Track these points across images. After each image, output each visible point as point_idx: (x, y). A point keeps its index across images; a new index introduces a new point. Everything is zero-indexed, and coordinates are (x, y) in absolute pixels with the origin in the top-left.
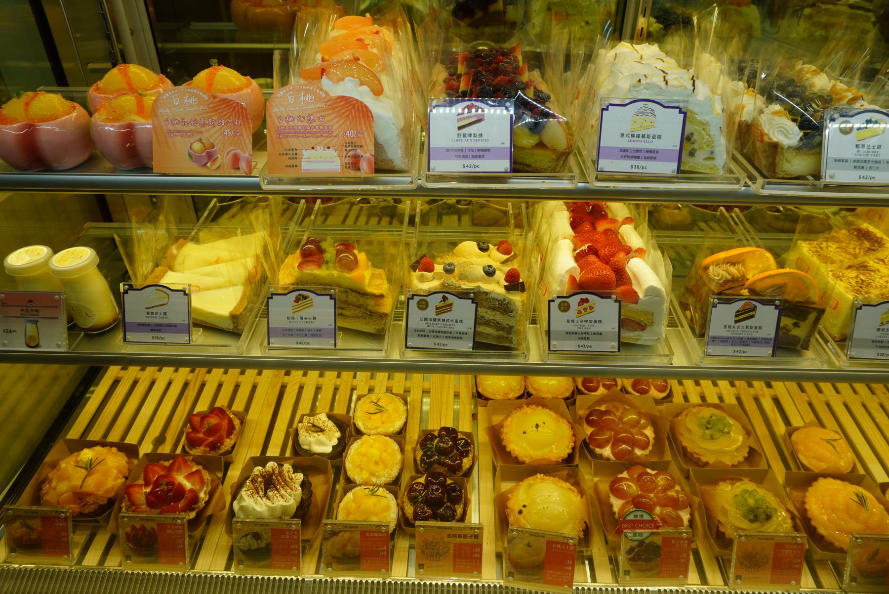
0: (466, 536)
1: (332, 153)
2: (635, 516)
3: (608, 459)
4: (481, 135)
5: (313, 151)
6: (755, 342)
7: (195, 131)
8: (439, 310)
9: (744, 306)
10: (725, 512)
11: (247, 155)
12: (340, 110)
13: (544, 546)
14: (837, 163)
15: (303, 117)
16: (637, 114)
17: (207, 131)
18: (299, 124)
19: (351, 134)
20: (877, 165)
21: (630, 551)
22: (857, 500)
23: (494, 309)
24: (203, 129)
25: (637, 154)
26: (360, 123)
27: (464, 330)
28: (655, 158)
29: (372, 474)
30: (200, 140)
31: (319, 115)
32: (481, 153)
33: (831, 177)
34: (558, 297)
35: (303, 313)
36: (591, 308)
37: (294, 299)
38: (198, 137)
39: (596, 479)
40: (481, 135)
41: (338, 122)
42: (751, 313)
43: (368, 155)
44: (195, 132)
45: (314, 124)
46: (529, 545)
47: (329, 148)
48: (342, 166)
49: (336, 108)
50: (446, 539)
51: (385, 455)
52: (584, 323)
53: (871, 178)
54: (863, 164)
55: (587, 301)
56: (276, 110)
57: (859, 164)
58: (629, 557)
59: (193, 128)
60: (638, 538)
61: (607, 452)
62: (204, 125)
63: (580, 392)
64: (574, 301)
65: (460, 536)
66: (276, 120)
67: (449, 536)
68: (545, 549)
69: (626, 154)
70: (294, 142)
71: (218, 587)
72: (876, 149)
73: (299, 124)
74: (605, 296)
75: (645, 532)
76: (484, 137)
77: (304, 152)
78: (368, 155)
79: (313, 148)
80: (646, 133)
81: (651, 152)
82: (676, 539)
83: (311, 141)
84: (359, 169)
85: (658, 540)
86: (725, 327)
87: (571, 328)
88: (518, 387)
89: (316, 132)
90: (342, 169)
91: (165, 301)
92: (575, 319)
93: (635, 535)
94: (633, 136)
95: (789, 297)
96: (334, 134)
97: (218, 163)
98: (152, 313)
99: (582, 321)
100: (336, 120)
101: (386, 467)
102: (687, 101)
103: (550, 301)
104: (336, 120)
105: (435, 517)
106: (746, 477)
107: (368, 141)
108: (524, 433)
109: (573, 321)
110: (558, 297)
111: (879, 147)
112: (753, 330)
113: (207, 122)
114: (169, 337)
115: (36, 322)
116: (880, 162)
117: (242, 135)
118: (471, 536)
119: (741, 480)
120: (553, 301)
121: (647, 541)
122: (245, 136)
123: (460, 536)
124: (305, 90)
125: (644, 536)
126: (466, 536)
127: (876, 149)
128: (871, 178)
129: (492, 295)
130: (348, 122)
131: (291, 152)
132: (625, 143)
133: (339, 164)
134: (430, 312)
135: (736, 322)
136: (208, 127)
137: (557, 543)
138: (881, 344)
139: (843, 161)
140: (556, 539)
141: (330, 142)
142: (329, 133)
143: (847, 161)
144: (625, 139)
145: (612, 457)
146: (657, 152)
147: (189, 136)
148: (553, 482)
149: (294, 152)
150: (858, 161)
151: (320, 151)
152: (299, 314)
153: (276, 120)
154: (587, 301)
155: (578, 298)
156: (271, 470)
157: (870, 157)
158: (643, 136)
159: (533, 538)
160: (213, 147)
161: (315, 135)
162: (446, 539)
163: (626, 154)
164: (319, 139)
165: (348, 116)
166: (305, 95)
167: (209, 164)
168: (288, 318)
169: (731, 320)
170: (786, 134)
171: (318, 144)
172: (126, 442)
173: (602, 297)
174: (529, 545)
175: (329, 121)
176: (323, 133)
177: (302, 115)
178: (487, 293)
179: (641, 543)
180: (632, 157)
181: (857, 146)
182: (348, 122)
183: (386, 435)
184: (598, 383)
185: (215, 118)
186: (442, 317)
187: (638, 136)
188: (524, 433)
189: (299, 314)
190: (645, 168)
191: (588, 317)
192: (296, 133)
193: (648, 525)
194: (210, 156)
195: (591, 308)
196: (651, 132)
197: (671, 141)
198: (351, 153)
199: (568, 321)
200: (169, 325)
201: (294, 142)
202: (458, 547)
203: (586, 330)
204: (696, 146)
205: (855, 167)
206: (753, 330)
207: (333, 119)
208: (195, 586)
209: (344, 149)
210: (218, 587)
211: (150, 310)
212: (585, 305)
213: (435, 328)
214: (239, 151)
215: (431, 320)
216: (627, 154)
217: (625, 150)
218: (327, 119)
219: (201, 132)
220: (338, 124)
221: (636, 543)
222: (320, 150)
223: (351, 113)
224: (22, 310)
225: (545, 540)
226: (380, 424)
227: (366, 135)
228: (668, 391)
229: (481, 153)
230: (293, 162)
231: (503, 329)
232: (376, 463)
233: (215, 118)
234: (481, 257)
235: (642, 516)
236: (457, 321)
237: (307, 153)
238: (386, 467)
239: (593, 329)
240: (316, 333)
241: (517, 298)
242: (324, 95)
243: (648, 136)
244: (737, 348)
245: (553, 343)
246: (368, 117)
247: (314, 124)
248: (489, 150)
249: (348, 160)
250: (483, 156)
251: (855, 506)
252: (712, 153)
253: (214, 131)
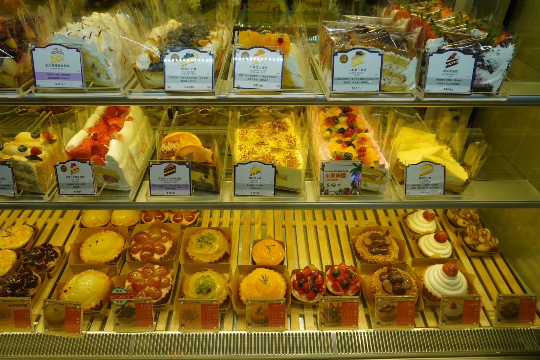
0: (19, 305)
2: (117, 291)
3: (138, 260)
6: (179, 187)
9: (168, 165)
10: (188, 288)
13: (64, 310)
14: (172, 79)
20: (195, 79)
21: (117, 312)
22: (262, 279)
23: (23, 171)
27: (7, 183)
28: (459, 84)
33: (169, 87)
34: (60, 163)
42: (174, 170)
46: (55, 310)
50: (9, 308)
53: (451, 90)
54: (186, 79)
57: (184, 79)
58: (117, 315)
60: (120, 304)
61: (137, 256)
63: (142, 222)
65: (16, 306)
67: (10, 305)
68: (64, 311)
71: (120, 347)
72: (193, 70)
74: (84, 162)
75: (124, 301)
80: (60, 63)
81: (65, 75)
82: (143, 304)
85: (133, 305)
86: (159, 178)
87: (69, 181)
88: (104, 220)
93: (118, 302)
94: (53, 65)
95: (195, 160)
102: (81, 45)
105: (12, 295)
106: (210, 268)
108: (90, 246)
110: (60, 163)
111: (195, 69)
112: (176, 180)
116: (196, 78)
118: (23, 305)
119: (207, 270)
120: (58, 166)
121: (126, 305)
123: (16, 306)
125: (124, 302)
126: (19, 305)
127: (193, 70)
128: (451, 90)
129: (19, 163)
132: (49, 70)
135: (165, 175)
137: (71, 308)
138: (252, 187)
139: (274, 77)
140: (70, 306)
143: (177, 77)
144: (48, 68)
145: (140, 259)
146: (69, 75)
148: (95, 274)
150: (183, 78)
157: (190, 75)
159: (57, 306)
162: (9, 308)
163: (251, 78)
169: (162, 174)
173: (82, 163)
174: (55, 310)
179: (123, 307)
180: (55, 78)
181: (182, 69)
183: (11, 249)
184: (152, 217)
187: (56, 66)
188: (90, 246)
190: (64, 84)
193: (125, 296)
195: (78, 169)
196: (63, 63)
197: (76, 68)
202: (16, 312)
203: (76, 182)
204: (98, 71)
205: (182, 81)
206: (176, 180)
208: (106, 347)
210: (120, 347)
212: (74, 167)
217: (50, 74)
221: (120, 307)
225: (64, 306)
226: (9, 243)
228: (193, 221)
231: (31, 183)
234: (33, 141)
235: (121, 291)
239: (80, 182)
241: (33, 165)
243: (62, 66)
244: (169, 191)
251: (260, 283)
252: (107, 75)
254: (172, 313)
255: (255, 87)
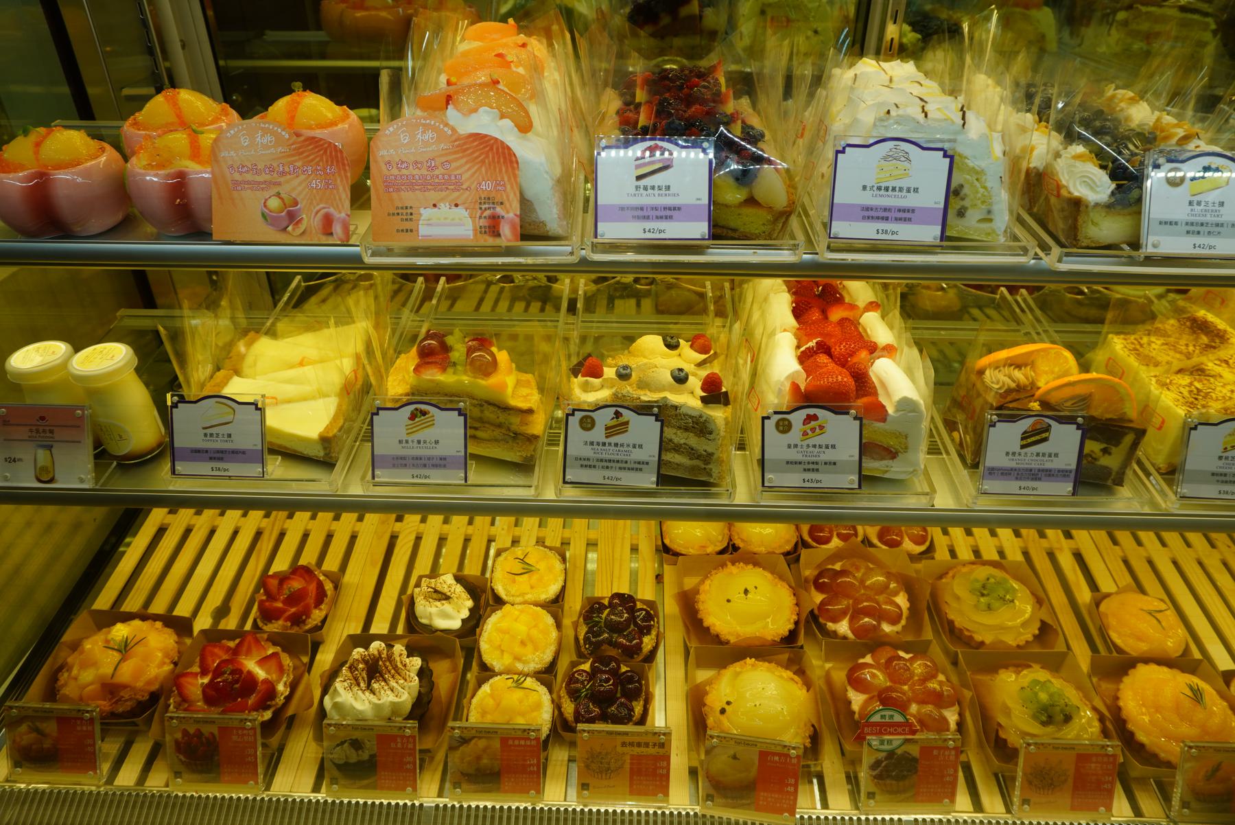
0: (647, 745)
1: (461, 212)
2: (882, 717)
3: (845, 638)
4: (668, 188)
5: (436, 210)
6: (1049, 474)
7: (270, 182)
8: (610, 431)
9: (1034, 424)
10: (1007, 712)
11: (343, 215)
12: (473, 153)
13: (756, 758)
14: (1163, 226)
15: (421, 163)
16: (885, 159)
17: (287, 182)
18: (415, 172)
19: (487, 186)
20: (1219, 229)
21: (876, 765)
22: (1190, 694)
23: (686, 429)
24: (282, 180)
25: (885, 214)
26: (501, 171)
27: (644, 458)
28: (910, 220)
29: (517, 658)
30: (278, 195)
31: (444, 159)
32: (668, 213)
33: (1155, 246)
34: (776, 413)
35: (420, 435)
36: (821, 427)
37: (409, 415)
38: (275, 190)
39: (828, 665)
40: (668, 188)
41: (469, 169)
42: (1044, 435)
43: (511, 215)
44: (270, 184)
45: (437, 172)
46: (735, 757)
47: (456, 205)
48: (475, 230)
49: (467, 149)
50: (620, 749)
51: (534, 632)
52: (811, 449)
53: (1210, 247)
54: (1199, 228)
55: (815, 417)
56: (383, 152)
57: (1194, 228)
58: (874, 773)
59: (268, 177)
60: (886, 747)
61: (843, 627)
62: (283, 173)
63: (806, 545)
64: (797, 418)
65: (639, 745)
66: (384, 167)
67: (624, 744)
68: (757, 762)
69: (869, 213)
70: (408, 198)
72: (1217, 208)
73: (415, 172)
74: (840, 411)
75: (897, 739)
76: (672, 190)
77: (422, 211)
78: (511, 215)
79: (435, 206)
80: (897, 184)
81: (904, 211)
82: (939, 748)
83: (433, 196)
84: (499, 235)
85: (914, 750)
86: (1007, 454)
87: (794, 455)
88: (720, 538)
89: (439, 184)
90: (475, 235)
91: (230, 418)
92: (799, 443)
93: (882, 743)
94: (879, 188)
95: (1096, 412)
96: (464, 186)
97: (303, 227)
98: (211, 435)
99: (808, 446)
100: (467, 166)
101: (536, 649)
102: (954, 141)
103: (764, 418)
104: (467, 166)
105: (604, 718)
106: (1036, 662)
107: (512, 196)
108: (729, 601)
109: (796, 446)
110: (776, 413)
111: (1222, 204)
112: (1046, 458)
113: (287, 170)
114: (234, 469)
115: (50, 448)
116: (1222, 225)
117: (336, 187)
118: (655, 745)
119: (1030, 666)
120: (768, 418)
121: (899, 752)
122: (341, 188)
123: (639, 745)
124: (424, 125)
125: (895, 744)
126: (647, 745)
127: (1217, 208)
128: (1210, 247)
129: (683, 410)
130: (483, 169)
131: (404, 211)
132: (869, 199)
133: (471, 227)
134: (598, 434)
135: (1023, 447)
136: (288, 177)
137: (774, 754)
138: (1223, 478)
139: (1171, 223)
140: (773, 749)
141: (458, 197)
142: (458, 185)
143: (1176, 223)
144: (868, 193)
145: (850, 635)
146: (913, 211)
147: (263, 189)
148: (769, 670)
149: (409, 211)
150: (1192, 224)
151: (445, 210)
152: (416, 437)
153: (384, 167)
154: (815, 417)
155: (803, 414)
156: (376, 653)
157: (1209, 218)
158: (894, 189)
159: (741, 748)
160: (296, 204)
161: (437, 187)
162: (620, 749)
163: (869, 213)
164: (444, 193)
165: (483, 162)
166: (424, 132)
167: (290, 228)
168: (400, 442)
169: (1015, 444)
170: (1092, 187)
171: (442, 200)
172: (175, 613)
173: (836, 413)
174: (735, 757)
175: (457, 168)
176: (449, 184)
177: (419, 159)
178: (676, 407)
179: (891, 754)
180: (878, 218)
181: (1191, 203)
182: (483, 169)
183: (536, 604)
184: (831, 532)
185: (299, 164)
186: (613, 440)
187: (887, 189)
188: (729, 601)
189: (416, 437)
190: (896, 233)
191: (817, 440)
192: (412, 185)
193: (900, 730)
194: (292, 217)
195: (821, 427)
196: (904, 184)
197: (933, 195)
198: (487, 213)
199: (789, 446)
200: (234, 452)
201: (408, 198)
202: (637, 760)
203: (814, 459)
204: (966, 203)
205: (1188, 232)
206: (1046, 458)
207: (462, 166)
209: (477, 206)
211: (208, 431)
212: (813, 424)
213: (604, 456)
214: (332, 210)
215: (598, 444)
216: (870, 213)
217: (868, 208)
218: (454, 165)
219: (279, 184)
220: (470, 173)
221: (884, 754)
222: (444, 208)
223: (487, 157)
224: (31, 431)
225: (757, 749)
226: (528, 589)
227: (508, 187)
228: (928, 544)
229: (668, 213)
230: (408, 225)
231: (699, 457)
232: (523, 643)
233: (299, 164)
234: (668, 356)
235: (892, 717)
236: (634, 446)
237: (426, 213)
238: (536, 649)
239: (823, 457)
240: (439, 462)
241: (718, 414)
242: (450, 132)
243: (901, 189)
244: (1023, 484)
245: (768, 476)
246: (511, 162)
247: (437, 172)
248: (679, 209)
249: (483, 222)
250: (671, 217)
251: (1188, 703)
252: (989, 212)
253: (297, 181)
254: (158, 701)
255: (880, 236)
